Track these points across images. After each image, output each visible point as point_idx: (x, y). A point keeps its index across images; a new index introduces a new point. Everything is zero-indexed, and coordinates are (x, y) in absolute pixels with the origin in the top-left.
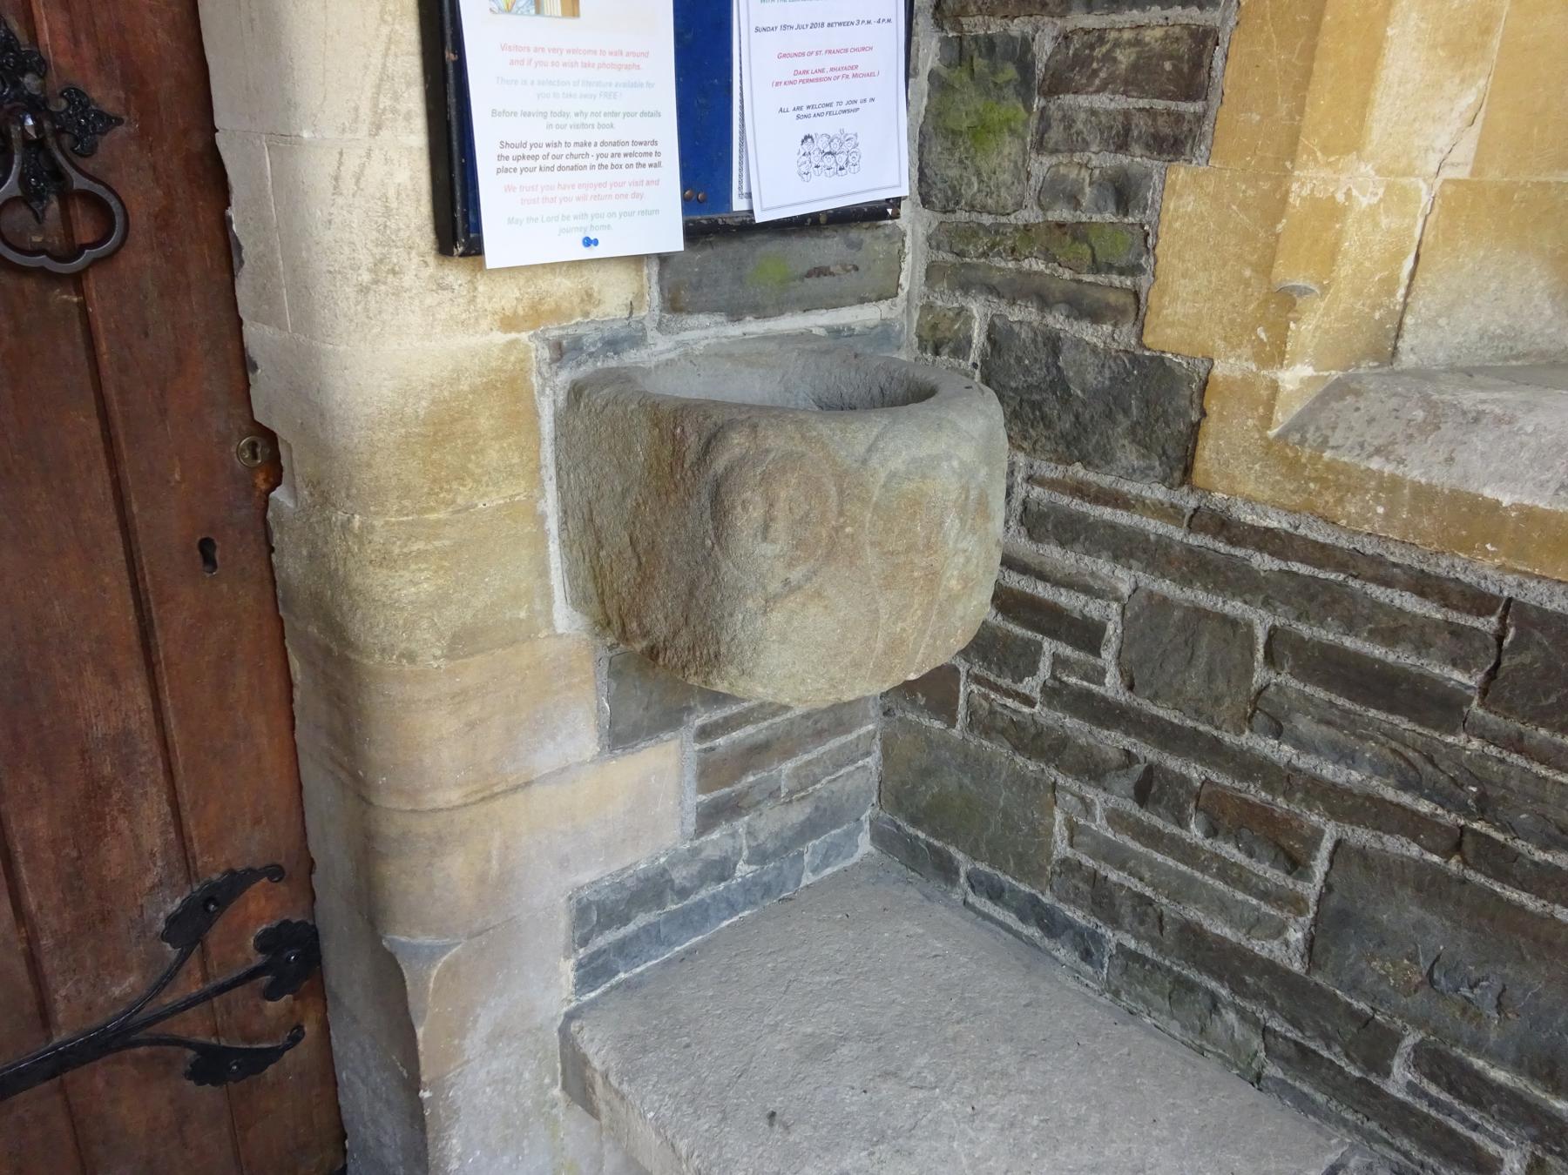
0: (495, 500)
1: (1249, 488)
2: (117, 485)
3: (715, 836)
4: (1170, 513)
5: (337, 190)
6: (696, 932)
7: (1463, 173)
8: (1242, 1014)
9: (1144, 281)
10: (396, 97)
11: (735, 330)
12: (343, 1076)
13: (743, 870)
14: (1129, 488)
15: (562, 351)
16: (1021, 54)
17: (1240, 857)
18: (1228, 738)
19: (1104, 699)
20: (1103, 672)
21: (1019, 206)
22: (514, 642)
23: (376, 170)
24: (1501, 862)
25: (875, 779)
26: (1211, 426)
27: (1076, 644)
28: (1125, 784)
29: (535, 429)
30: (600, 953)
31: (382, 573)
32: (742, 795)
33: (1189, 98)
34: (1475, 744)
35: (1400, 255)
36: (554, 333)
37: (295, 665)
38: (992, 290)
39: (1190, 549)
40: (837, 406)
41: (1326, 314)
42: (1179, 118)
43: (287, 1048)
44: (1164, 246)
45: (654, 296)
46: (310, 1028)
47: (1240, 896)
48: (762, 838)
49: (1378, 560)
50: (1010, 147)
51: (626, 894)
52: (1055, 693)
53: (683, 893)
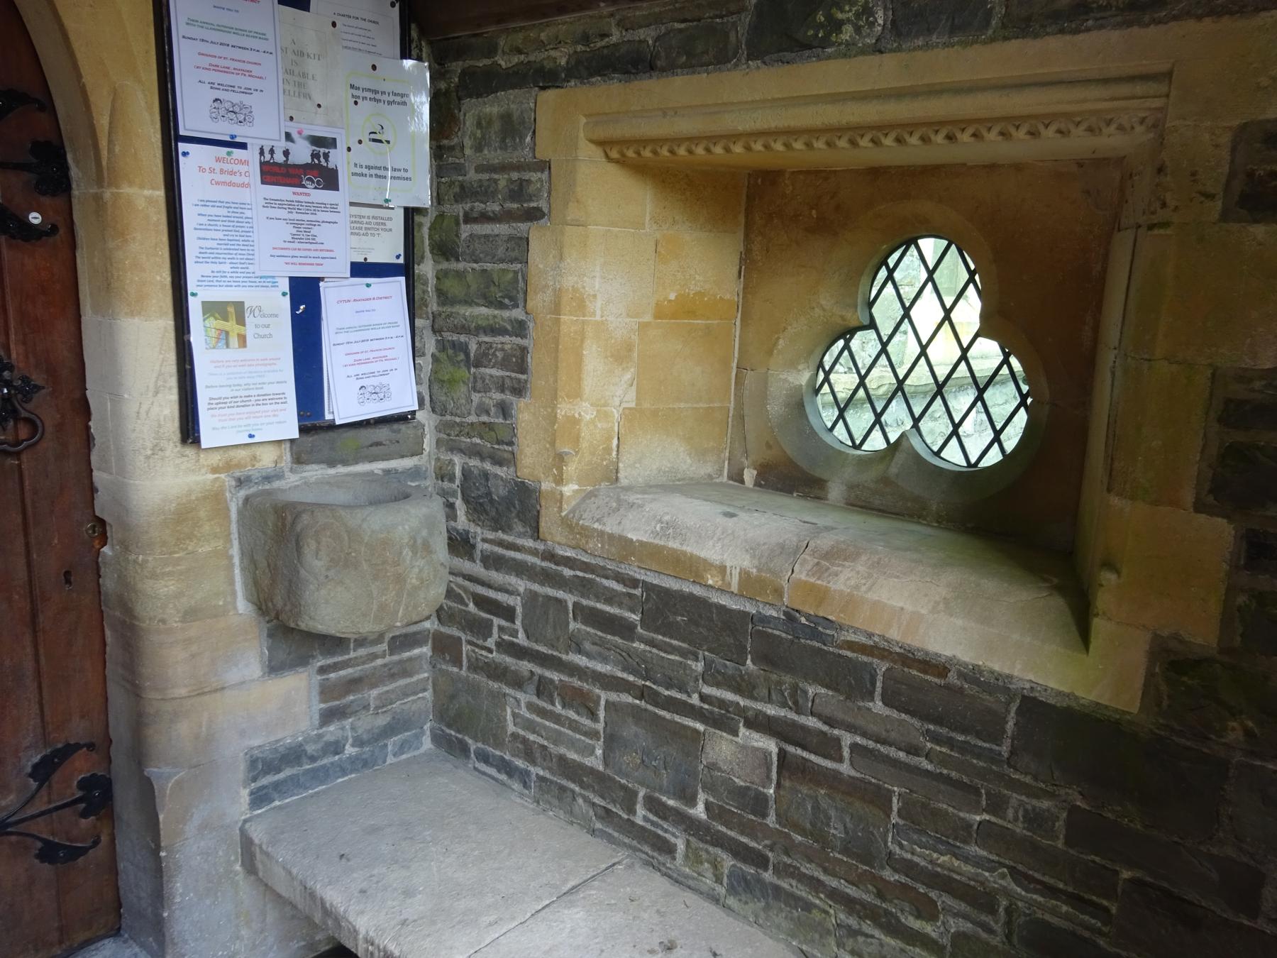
0: (207, 548)
1: (558, 539)
2: (27, 544)
3: (332, 728)
4: (534, 552)
5: (138, 417)
6: (322, 783)
7: (633, 405)
8: (586, 799)
9: (515, 447)
10: (165, 381)
11: (332, 471)
12: (121, 866)
13: (350, 750)
14: (520, 541)
15: (240, 482)
16: (464, 348)
17: (575, 717)
18: (564, 657)
19: (518, 645)
20: (517, 631)
21: (469, 414)
22: (216, 616)
23: (155, 409)
24: (655, 699)
25: (430, 705)
26: (543, 512)
27: (507, 620)
28: (532, 688)
29: (228, 517)
30: (264, 787)
31: (151, 582)
32: (346, 706)
33: (522, 373)
34: (642, 646)
35: (610, 439)
36: (238, 474)
37: (108, 633)
38: (461, 451)
39: (543, 569)
40: (375, 502)
41: (580, 462)
42: (519, 381)
43: (91, 848)
44: (519, 432)
45: (288, 457)
46: (104, 838)
47: (578, 736)
48: (360, 732)
49: (604, 568)
50: (463, 389)
51: (278, 755)
52: (503, 646)
53: (313, 759)
